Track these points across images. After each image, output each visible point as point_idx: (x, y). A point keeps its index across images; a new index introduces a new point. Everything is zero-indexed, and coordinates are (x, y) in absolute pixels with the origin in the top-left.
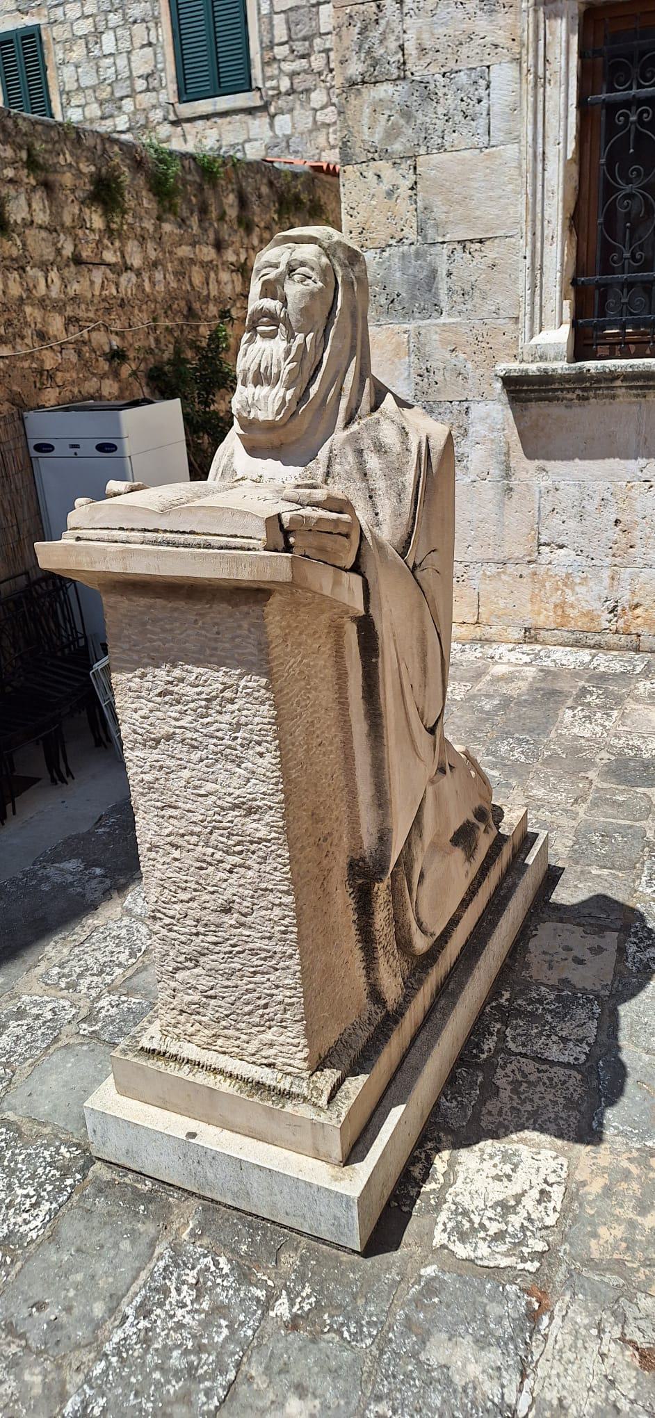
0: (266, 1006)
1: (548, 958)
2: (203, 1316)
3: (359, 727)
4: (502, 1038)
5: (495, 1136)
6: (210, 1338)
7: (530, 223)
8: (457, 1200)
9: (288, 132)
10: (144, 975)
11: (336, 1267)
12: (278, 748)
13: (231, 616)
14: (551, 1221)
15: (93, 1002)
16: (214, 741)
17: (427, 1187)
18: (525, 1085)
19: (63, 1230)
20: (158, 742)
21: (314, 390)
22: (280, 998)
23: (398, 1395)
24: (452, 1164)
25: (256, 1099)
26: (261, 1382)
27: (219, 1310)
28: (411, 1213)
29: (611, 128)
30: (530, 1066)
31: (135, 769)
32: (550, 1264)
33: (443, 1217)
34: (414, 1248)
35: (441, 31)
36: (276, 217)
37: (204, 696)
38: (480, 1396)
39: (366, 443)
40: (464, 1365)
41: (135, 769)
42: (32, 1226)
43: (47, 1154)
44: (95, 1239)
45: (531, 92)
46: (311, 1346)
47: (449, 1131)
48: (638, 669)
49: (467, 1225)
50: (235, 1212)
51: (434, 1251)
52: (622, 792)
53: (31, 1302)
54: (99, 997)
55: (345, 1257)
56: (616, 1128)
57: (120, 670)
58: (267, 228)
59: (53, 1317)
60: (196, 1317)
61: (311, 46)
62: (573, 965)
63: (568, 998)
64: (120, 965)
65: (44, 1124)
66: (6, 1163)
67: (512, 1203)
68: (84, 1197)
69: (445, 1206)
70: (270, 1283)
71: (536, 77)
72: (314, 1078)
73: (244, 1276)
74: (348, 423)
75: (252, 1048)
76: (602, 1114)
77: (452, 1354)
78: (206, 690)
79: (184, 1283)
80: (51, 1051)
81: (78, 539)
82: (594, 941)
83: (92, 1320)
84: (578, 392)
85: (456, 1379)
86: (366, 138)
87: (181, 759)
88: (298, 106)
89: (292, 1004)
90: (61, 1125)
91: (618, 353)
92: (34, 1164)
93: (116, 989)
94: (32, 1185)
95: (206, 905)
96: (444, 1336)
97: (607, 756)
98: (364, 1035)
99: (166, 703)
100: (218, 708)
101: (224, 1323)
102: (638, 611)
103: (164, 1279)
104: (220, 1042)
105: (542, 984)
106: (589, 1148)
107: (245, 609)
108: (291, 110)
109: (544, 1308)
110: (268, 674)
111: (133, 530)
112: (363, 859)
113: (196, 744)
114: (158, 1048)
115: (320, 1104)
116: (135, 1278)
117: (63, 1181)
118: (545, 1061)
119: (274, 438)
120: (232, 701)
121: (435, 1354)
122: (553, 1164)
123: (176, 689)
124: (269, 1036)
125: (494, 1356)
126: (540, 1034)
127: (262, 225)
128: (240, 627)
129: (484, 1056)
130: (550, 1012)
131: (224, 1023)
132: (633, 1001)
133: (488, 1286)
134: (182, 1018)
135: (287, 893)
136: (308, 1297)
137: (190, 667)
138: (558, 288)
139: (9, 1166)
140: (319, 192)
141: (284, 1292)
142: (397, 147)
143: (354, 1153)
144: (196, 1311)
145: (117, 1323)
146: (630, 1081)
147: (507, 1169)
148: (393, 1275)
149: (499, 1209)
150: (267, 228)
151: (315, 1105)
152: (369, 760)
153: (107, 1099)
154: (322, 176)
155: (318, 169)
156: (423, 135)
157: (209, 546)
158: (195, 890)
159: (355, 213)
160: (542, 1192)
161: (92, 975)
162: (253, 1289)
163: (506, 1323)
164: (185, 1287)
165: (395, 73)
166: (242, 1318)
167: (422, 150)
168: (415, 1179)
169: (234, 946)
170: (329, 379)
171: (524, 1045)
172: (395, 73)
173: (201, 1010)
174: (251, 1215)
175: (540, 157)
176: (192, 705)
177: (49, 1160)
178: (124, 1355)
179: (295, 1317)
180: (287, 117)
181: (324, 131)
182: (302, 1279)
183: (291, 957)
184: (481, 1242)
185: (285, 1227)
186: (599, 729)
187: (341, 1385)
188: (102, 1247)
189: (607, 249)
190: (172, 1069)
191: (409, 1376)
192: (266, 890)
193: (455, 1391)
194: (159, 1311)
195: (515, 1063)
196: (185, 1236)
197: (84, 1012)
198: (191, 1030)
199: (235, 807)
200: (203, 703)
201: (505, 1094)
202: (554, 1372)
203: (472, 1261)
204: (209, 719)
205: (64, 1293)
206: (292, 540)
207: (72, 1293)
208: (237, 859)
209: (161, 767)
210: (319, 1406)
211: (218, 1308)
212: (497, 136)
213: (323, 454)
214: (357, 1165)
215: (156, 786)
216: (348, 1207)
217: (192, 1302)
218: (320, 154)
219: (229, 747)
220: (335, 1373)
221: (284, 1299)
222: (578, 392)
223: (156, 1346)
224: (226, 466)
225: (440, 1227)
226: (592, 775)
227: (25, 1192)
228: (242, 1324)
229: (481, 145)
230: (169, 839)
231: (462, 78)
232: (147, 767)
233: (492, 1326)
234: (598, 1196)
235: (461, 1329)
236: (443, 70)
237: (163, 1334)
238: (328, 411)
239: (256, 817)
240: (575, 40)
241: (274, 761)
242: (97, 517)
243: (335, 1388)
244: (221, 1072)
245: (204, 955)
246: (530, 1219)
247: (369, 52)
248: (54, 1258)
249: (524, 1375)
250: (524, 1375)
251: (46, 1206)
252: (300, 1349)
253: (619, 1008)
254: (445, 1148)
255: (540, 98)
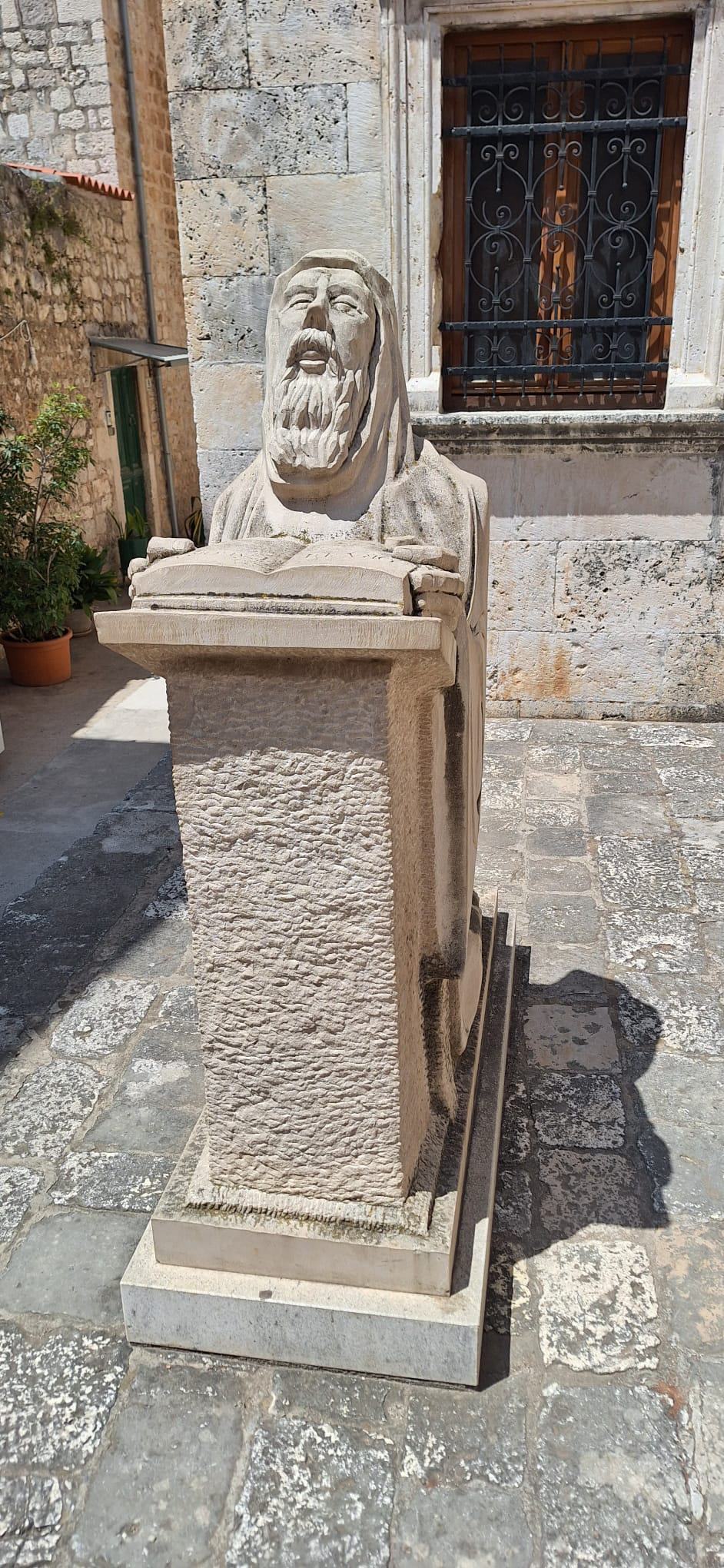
0: (353, 1133)
1: (548, 1042)
2: (328, 1494)
3: (440, 808)
4: (535, 1133)
5: (564, 1237)
6: (347, 1517)
7: (395, 260)
8: (552, 1310)
9: (26, 135)
10: (107, 1124)
11: (452, 1409)
12: (390, 838)
13: (344, 691)
14: (652, 1313)
15: (56, 1164)
16: (309, 836)
17: (517, 1303)
18: (573, 1178)
19: (122, 1435)
20: (232, 842)
21: (365, 434)
22: (371, 1121)
23: (572, 1528)
24: (532, 1273)
25: (344, 1239)
26: (420, 1552)
27: (343, 1484)
28: (509, 1334)
29: (477, 165)
30: (572, 1158)
31: (198, 877)
32: (667, 1357)
33: (544, 1331)
34: (526, 1370)
35: (290, 39)
36: (28, 232)
37: (300, 785)
38: (653, 1508)
39: (418, 495)
40: (626, 1480)
41: (198, 877)
42: (83, 1438)
43: (68, 1350)
44: (167, 1437)
45: (393, 118)
46: (460, 1498)
47: (517, 1240)
48: (526, 736)
49: (573, 1334)
50: (319, 1372)
51: (548, 1368)
52: (556, 863)
53: (117, 1527)
54: (63, 1158)
55: (458, 1395)
56: (678, 1206)
57: (185, 761)
58: (19, 244)
59: (151, 1539)
60: (321, 1498)
61: (48, 37)
62: (577, 1047)
63: (585, 1083)
64: (74, 1116)
65: (52, 1317)
66: (20, 1372)
67: (608, 1302)
68: (134, 1392)
69: (542, 1319)
70: (388, 1441)
71: (398, 100)
72: (408, 1205)
73: (357, 1441)
74: (398, 471)
75: (333, 1183)
76: (660, 1194)
77: (608, 1473)
78: (304, 777)
79: (292, 1462)
80: (26, 1229)
81: (155, 607)
82: (586, 1019)
83: (198, 1531)
84: (452, 445)
85: (623, 1495)
86: (206, 151)
87: (262, 861)
88: (36, 107)
89: (386, 1126)
90: (74, 1313)
91: (488, 405)
92: (57, 1365)
93: (79, 1144)
94: (64, 1390)
95: (285, 1026)
96: (594, 1455)
97: (529, 827)
98: (439, 1149)
99: (247, 796)
100: (317, 798)
101: (355, 1497)
102: (518, 676)
103: (267, 1463)
104: (291, 1182)
105: (553, 1070)
106: (660, 1231)
107: (362, 683)
108: (28, 110)
109: (680, 1403)
110: (384, 755)
111: (227, 595)
112: (437, 956)
113: (284, 841)
114: (212, 1201)
115: (420, 1231)
116: (232, 1471)
117: (102, 1378)
118: (584, 1150)
119: (322, 488)
120: (336, 789)
121: (593, 1474)
122: (632, 1254)
123: (263, 779)
124: (356, 1165)
125: (650, 1463)
126: (570, 1122)
127: (14, 240)
128: (354, 704)
129: (523, 1154)
130: (571, 1098)
131: (299, 1159)
132: (647, 1075)
133: (617, 1393)
134: (243, 1162)
135: (390, 1001)
136: (436, 1446)
137: (284, 753)
138: (427, 333)
139: (25, 1374)
140: (73, 208)
141: (408, 1448)
142: (243, 164)
143: (459, 1279)
144: (318, 1491)
145: (231, 1526)
146: (674, 1157)
147: (590, 1267)
148: (514, 1404)
149: (598, 1311)
150: (19, 244)
151: (413, 1234)
152: (448, 845)
153: (147, 1269)
154: (75, 188)
155: (72, 180)
156: (273, 154)
157: (333, 612)
158: (271, 1011)
159: (195, 235)
160: (633, 1285)
161: (44, 1133)
162: (372, 1452)
163: (649, 1426)
164: (295, 1468)
165: (239, 81)
166: (372, 1486)
167: (273, 171)
168: (501, 1297)
169: (316, 1069)
170: (377, 421)
171: (559, 1137)
172: (239, 81)
173: (269, 1148)
174: (341, 1371)
175: (404, 189)
176: (283, 797)
177: (73, 1357)
178: (254, 1560)
179: (430, 1472)
180: (23, 117)
181: (69, 138)
182: (421, 1428)
183: (388, 1072)
184: (593, 1350)
185: (383, 1376)
186: (509, 800)
187: (507, 1531)
188: (179, 1444)
189: (474, 292)
190: (233, 1223)
191: (574, 1505)
192: (363, 1000)
193: (627, 1508)
194: (275, 1501)
195: (555, 1156)
196: (272, 1410)
197: (51, 1178)
198: (253, 1174)
199: (334, 909)
200: (299, 793)
201: (557, 1190)
202: (713, 1465)
203: (591, 1370)
204: (304, 812)
205: (153, 1507)
206: (421, 603)
207: (163, 1505)
208: (327, 970)
209: (235, 872)
210: (493, 1561)
211: (340, 1481)
212: (357, 162)
213: (375, 506)
214: (463, 1292)
215: (226, 894)
216: (466, 1338)
217: (310, 1482)
218: (65, 163)
219: (329, 842)
220: (495, 1520)
221: (410, 1455)
222: (452, 445)
223: (287, 1541)
224: (255, 520)
225: (545, 1342)
226: (520, 847)
227: (59, 1401)
228: (375, 1493)
229: (339, 170)
230: (239, 955)
231: (316, 94)
232: (215, 873)
233: (637, 1432)
234: (686, 1278)
235: (608, 1443)
236: (294, 83)
237: (290, 1525)
238: (379, 457)
239: (357, 918)
240: (438, 65)
241: (384, 854)
242: (178, 582)
243: (503, 1537)
244: (296, 1216)
245: (277, 1084)
246: (633, 1316)
247: (208, 53)
248: (126, 1470)
249: (686, 1476)
250: (686, 1476)
251: (92, 1412)
252: (449, 1505)
253: (638, 1083)
254: (519, 1259)
255: (403, 124)
